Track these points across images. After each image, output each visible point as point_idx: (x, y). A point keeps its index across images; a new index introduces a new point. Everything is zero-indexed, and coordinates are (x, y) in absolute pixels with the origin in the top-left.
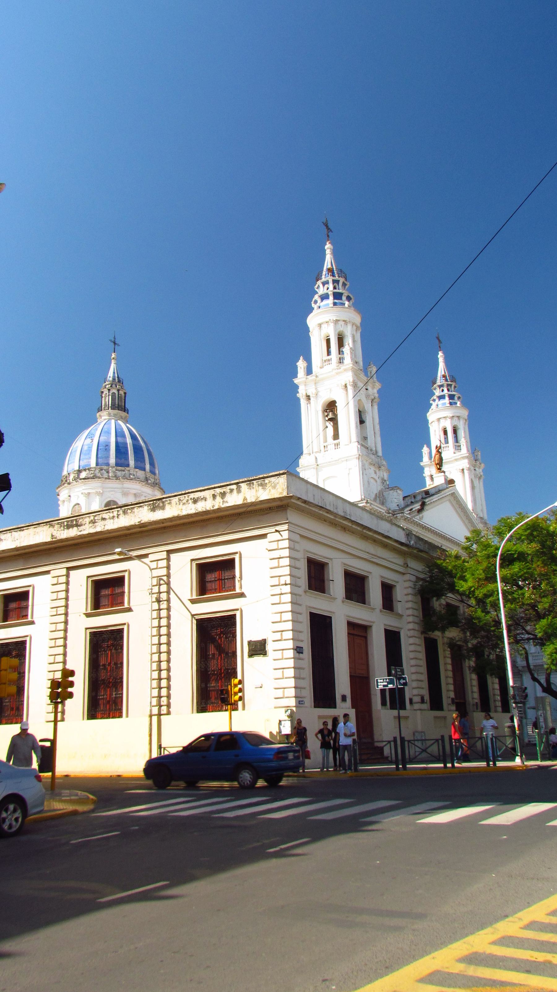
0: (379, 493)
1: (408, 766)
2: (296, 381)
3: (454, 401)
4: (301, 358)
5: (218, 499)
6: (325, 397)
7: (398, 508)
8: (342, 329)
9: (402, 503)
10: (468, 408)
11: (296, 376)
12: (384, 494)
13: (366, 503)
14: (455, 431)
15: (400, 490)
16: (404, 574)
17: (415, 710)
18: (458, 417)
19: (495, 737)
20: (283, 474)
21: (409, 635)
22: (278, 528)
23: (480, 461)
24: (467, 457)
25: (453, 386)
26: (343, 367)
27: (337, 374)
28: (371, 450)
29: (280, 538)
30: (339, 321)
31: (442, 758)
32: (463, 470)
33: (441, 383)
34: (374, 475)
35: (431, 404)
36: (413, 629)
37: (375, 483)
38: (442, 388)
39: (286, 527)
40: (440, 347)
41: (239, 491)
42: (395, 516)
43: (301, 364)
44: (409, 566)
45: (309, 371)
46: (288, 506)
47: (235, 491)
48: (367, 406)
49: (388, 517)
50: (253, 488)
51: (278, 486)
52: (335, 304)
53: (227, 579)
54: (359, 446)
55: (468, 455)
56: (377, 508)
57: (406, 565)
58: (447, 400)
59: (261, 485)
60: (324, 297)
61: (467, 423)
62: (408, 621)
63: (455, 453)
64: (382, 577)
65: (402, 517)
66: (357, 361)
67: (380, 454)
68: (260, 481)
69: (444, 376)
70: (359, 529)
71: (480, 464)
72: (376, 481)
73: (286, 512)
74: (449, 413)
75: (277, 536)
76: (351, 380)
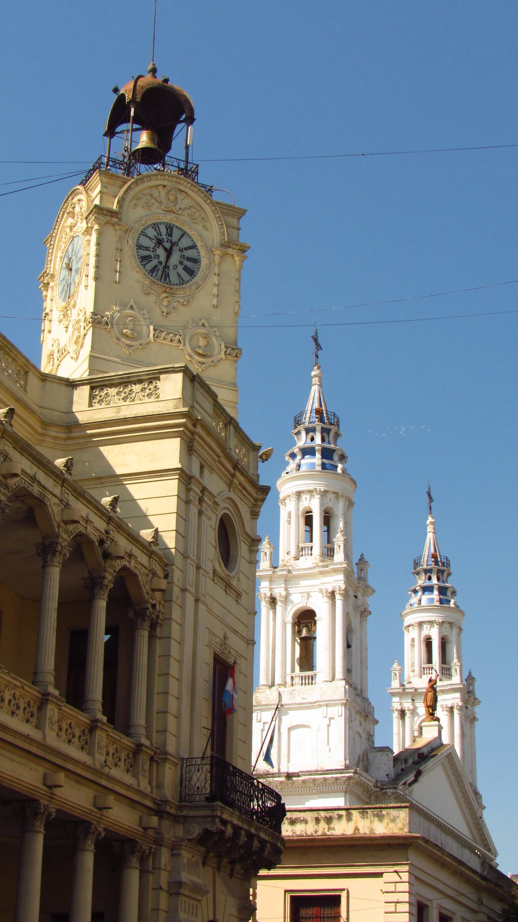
0: (363, 754)
3: (446, 598)
5: (323, 825)
6: (298, 602)
7: (387, 779)
8: (330, 505)
9: (392, 772)
12: (369, 757)
13: (354, 773)
14: (327, 519)
16: (475, 912)
18: (451, 624)
20: (405, 807)
22: (396, 868)
27: (322, 573)
29: (399, 879)
32: (333, 593)
33: (311, 425)
35: (288, 463)
38: (428, 574)
39: (406, 868)
41: (349, 818)
42: (384, 791)
44: (484, 903)
46: (410, 845)
47: (344, 819)
49: (375, 792)
50: (367, 818)
51: (398, 821)
53: (328, 917)
54: (347, 687)
57: (480, 902)
58: (317, 459)
59: (378, 816)
65: (393, 793)
68: (376, 811)
70: (453, 863)
73: (407, 852)
74: (318, 485)
75: (394, 877)
76: (343, 587)
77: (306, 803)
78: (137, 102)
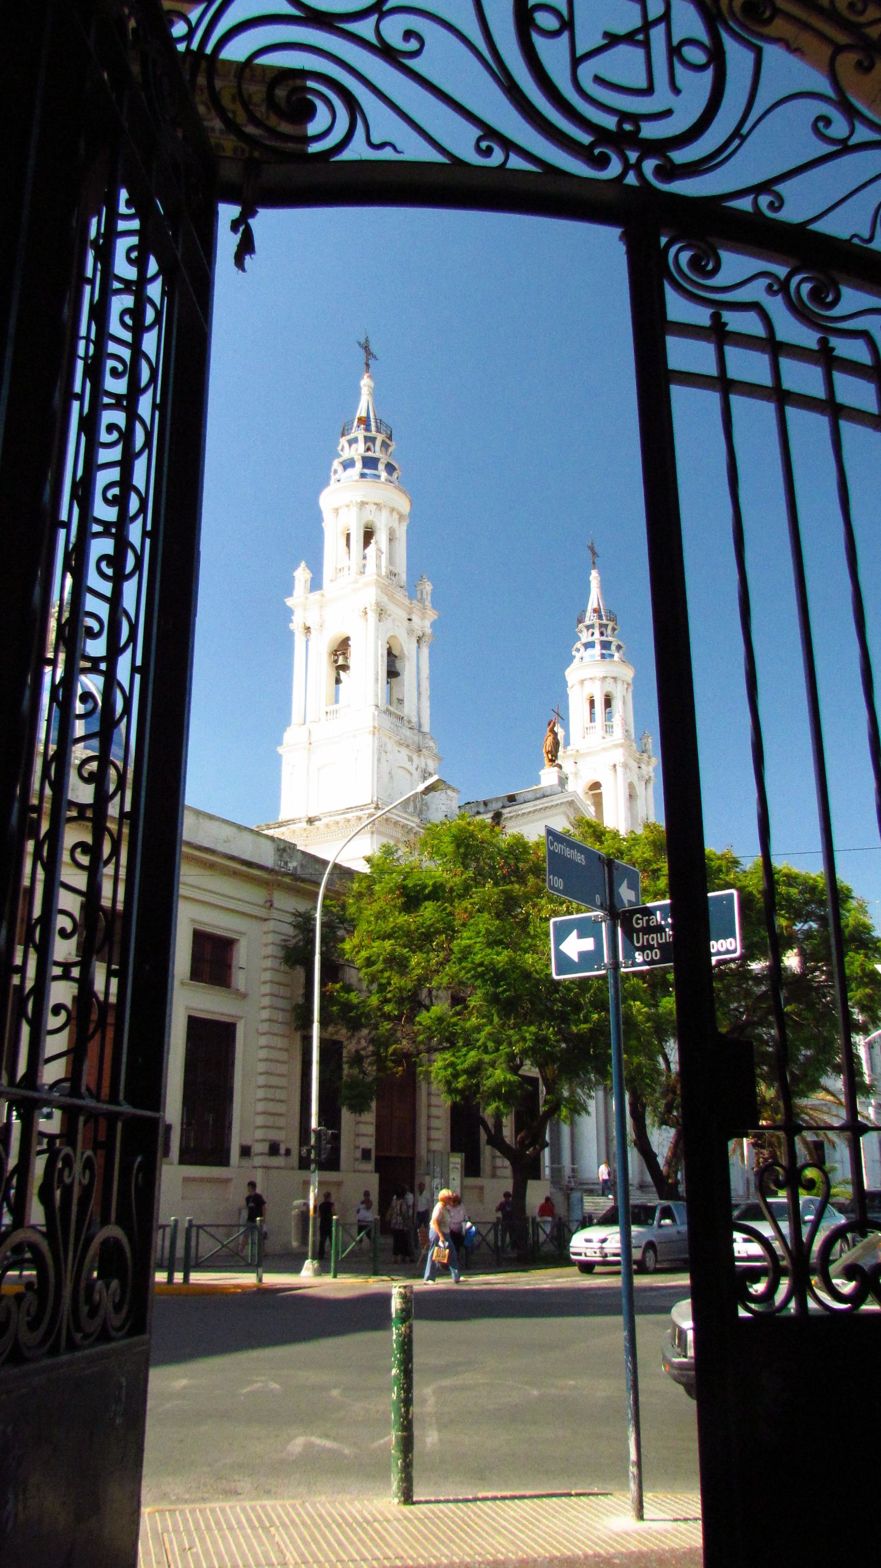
1: (34, 1273)
2: (289, 602)
3: (609, 652)
4: (303, 564)
8: (371, 518)
10: (635, 667)
11: (289, 592)
13: (375, 808)
14: (608, 702)
15: (454, 790)
16: (266, 920)
17: (255, 1167)
18: (615, 679)
19: (199, 1227)
21: (261, 1031)
23: (651, 754)
24: (622, 745)
25: (610, 628)
26: (363, 579)
28: (409, 722)
30: (367, 503)
31: (166, 1263)
32: (615, 766)
34: (407, 765)
35: (574, 657)
36: (270, 1020)
37: (408, 776)
38: (591, 631)
40: (594, 563)
43: (302, 575)
45: (316, 584)
48: (408, 647)
52: (363, 476)
55: (622, 741)
56: (399, 819)
58: (597, 650)
60: (348, 464)
61: (630, 690)
62: (262, 1005)
63: (604, 738)
64: (193, 921)
66: (396, 571)
67: (426, 728)
69: (597, 611)
71: (649, 757)
72: (411, 774)
77: (635, 1150)
78: (814, 1274)
